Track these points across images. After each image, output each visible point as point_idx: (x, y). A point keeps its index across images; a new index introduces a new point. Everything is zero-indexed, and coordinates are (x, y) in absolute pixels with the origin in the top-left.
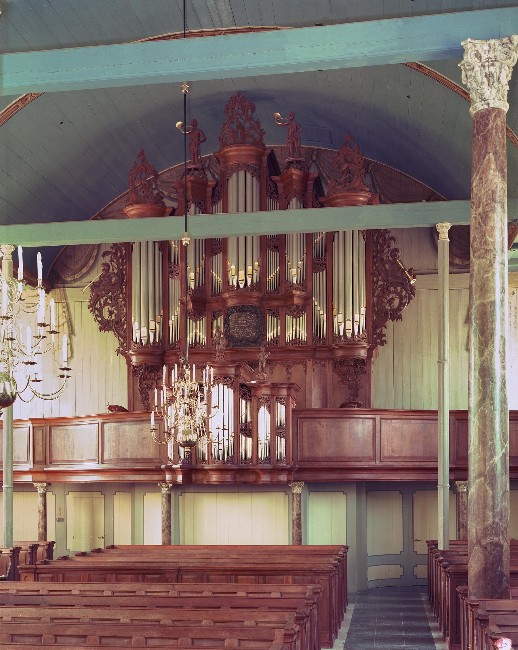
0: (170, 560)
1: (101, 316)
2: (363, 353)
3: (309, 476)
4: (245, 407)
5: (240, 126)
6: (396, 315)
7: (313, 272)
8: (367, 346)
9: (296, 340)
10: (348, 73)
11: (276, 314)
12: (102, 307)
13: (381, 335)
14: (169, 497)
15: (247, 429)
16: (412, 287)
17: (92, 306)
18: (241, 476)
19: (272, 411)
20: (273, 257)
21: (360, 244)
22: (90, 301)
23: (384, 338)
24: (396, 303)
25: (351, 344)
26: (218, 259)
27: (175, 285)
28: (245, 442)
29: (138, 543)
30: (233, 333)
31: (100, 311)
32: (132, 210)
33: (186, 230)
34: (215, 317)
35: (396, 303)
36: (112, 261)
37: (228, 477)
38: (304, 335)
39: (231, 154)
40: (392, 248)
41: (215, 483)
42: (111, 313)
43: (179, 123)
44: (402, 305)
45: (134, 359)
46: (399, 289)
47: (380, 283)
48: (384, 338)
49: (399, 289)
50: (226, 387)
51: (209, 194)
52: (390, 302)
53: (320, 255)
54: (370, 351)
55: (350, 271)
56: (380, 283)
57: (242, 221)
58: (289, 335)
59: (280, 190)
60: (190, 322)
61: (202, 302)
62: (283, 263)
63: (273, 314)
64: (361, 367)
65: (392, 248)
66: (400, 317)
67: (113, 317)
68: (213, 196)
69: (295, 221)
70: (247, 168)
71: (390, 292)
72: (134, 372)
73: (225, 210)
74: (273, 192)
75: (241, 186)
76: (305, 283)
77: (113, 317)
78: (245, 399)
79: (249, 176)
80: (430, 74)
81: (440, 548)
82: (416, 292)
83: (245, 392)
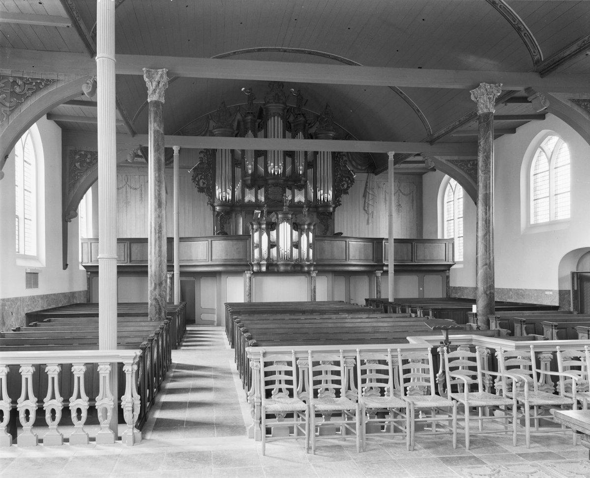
0: (311, 307)
1: (199, 185)
2: (331, 209)
3: (320, 268)
4: (295, 233)
5: (277, 94)
6: (346, 192)
7: (308, 169)
8: (333, 206)
9: (300, 202)
10: (352, 86)
11: (290, 188)
12: (199, 180)
13: (339, 201)
14: (250, 278)
15: (296, 245)
16: (353, 179)
17: (194, 179)
18: (295, 268)
19: (308, 236)
20: (289, 160)
21: (330, 156)
22: (193, 176)
23: (340, 203)
24: (345, 186)
25: (326, 204)
26: (261, 160)
27: (238, 171)
28: (295, 251)
29: (255, 300)
30: (271, 197)
31: (198, 182)
32: (216, 131)
33: (249, 143)
34: (259, 188)
35: (345, 186)
36: (204, 156)
37: (289, 268)
38: (303, 200)
39: (271, 107)
40: (344, 160)
41: (281, 271)
42: (204, 183)
43: (243, 89)
44: (348, 187)
45: (218, 208)
46: (347, 179)
47: (339, 176)
48: (340, 203)
49: (347, 179)
50: (288, 224)
51: (257, 126)
52: (343, 185)
53: (312, 162)
54: (334, 208)
55: (325, 168)
56: (339, 176)
57: (276, 142)
58: (296, 200)
59: (293, 127)
60: (247, 190)
61: (256, 181)
62: (293, 163)
63: (288, 189)
64: (331, 215)
65: (344, 160)
66: (347, 193)
67: (205, 185)
68: (259, 127)
69: (300, 144)
70: (279, 115)
71: (343, 181)
72: (217, 215)
73: (266, 137)
74: (290, 129)
75: (276, 123)
76: (305, 173)
77: (205, 185)
78: (295, 230)
79: (279, 118)
80: (405, 99)
81: (390, 301)
82: (355, 182)
83: (296, 226)
